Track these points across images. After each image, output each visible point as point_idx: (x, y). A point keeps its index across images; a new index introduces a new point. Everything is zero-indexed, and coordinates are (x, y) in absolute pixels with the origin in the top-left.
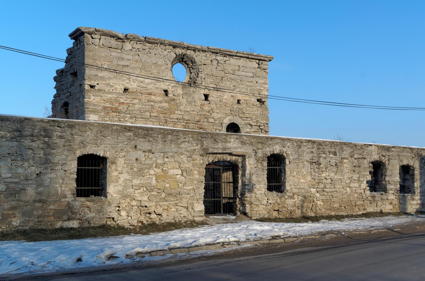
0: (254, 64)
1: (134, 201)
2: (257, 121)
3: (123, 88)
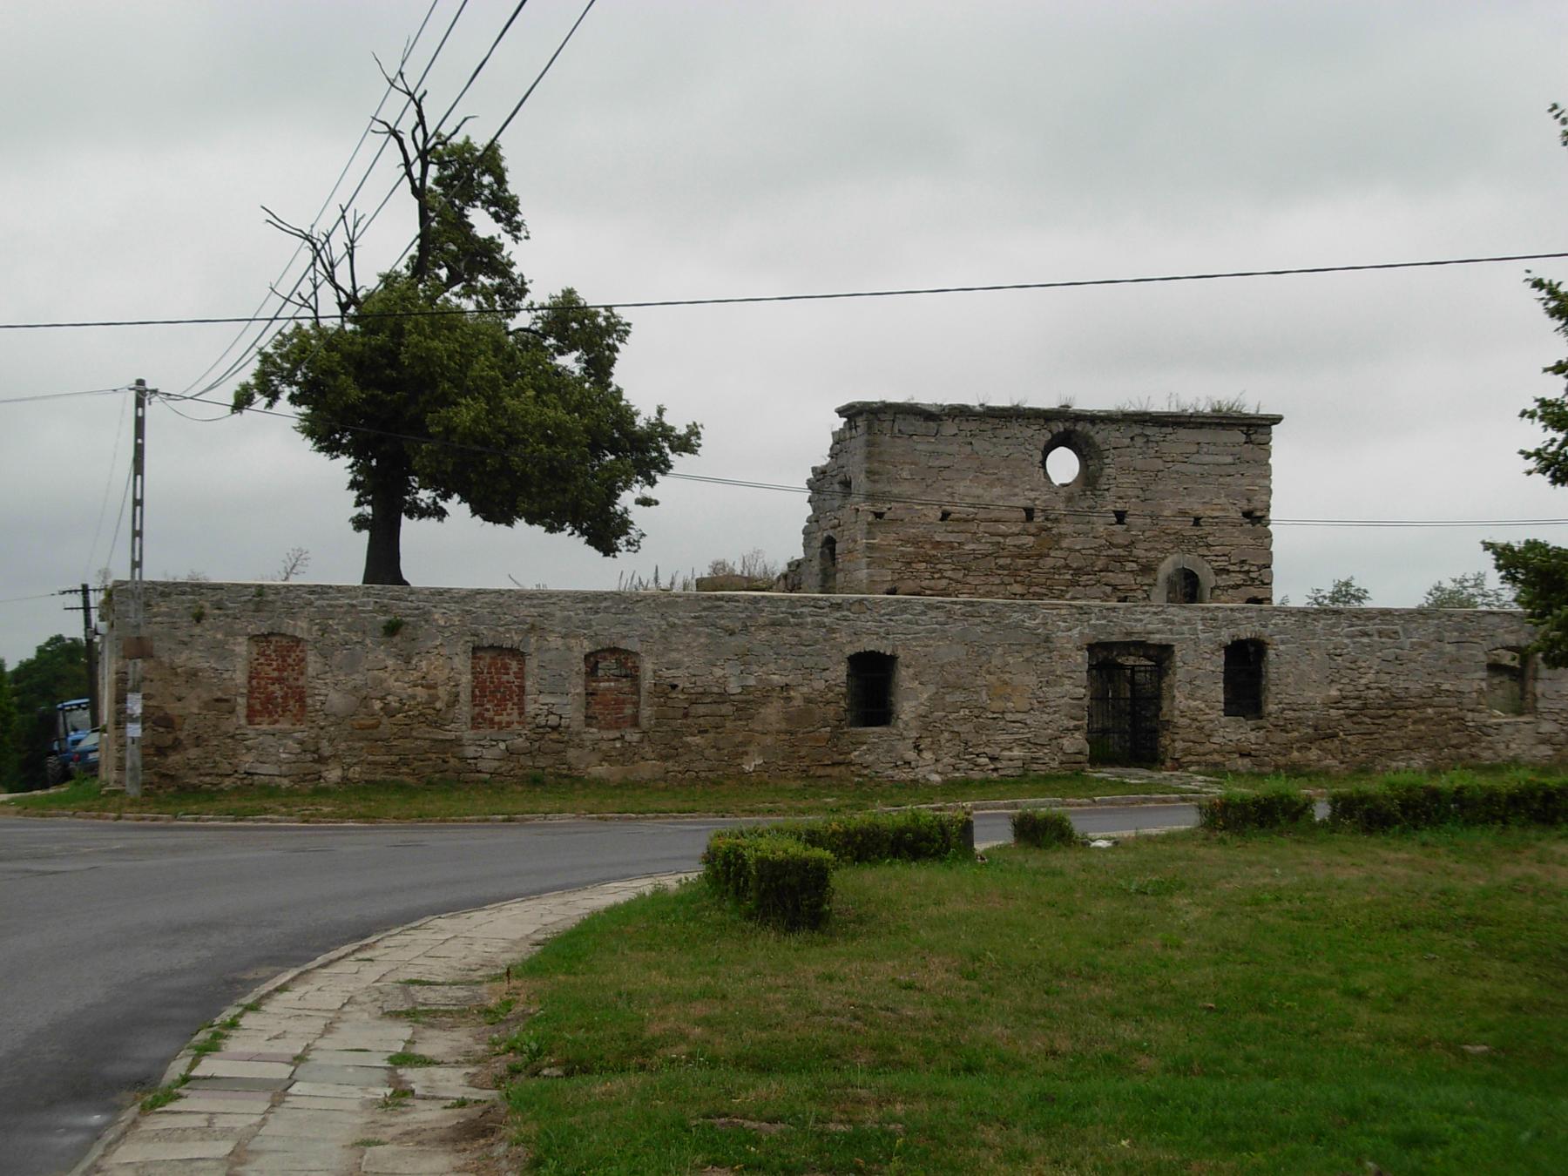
0: (1238, 436)
1: (492, 1003)
2: (1243, 562)
3: (940, 515)
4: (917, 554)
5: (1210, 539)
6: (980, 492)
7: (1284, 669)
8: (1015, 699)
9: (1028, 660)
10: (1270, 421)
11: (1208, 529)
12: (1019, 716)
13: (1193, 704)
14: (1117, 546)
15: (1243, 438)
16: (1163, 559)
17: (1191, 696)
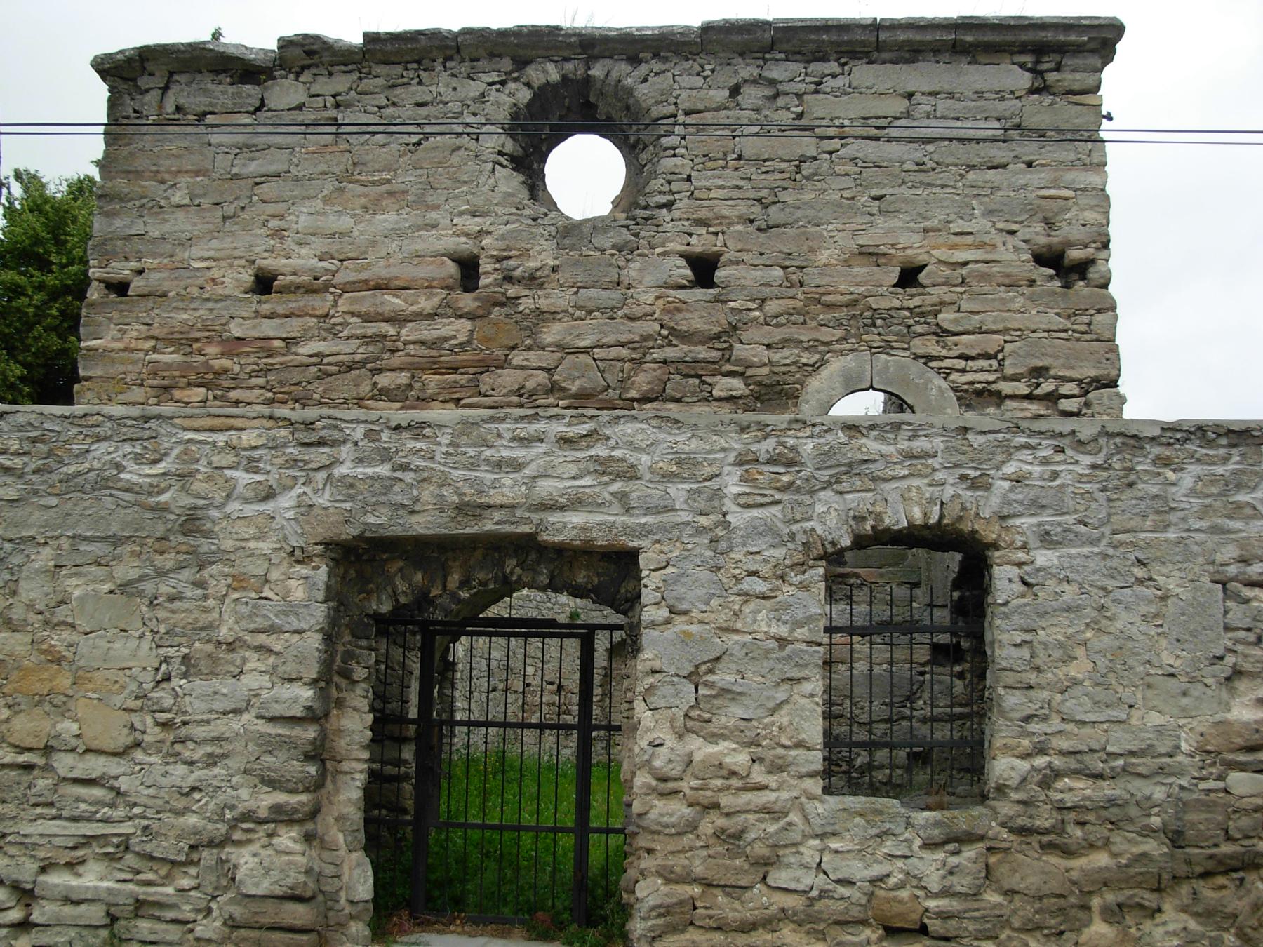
2: (1039, 372)
3: (248, 277)
4: (185, 369)
5: (946, 318)
6: (346, 222)
7: (1052, 632)
8: (80, 708)
9: (124, 588)
10: (1100, 39)
11: (938, 293)
12: (95, 766)
13: (702, 749)
14: (686, 337)
15: (1024, 80)
16: (815, 368)
17: (694, 723)
